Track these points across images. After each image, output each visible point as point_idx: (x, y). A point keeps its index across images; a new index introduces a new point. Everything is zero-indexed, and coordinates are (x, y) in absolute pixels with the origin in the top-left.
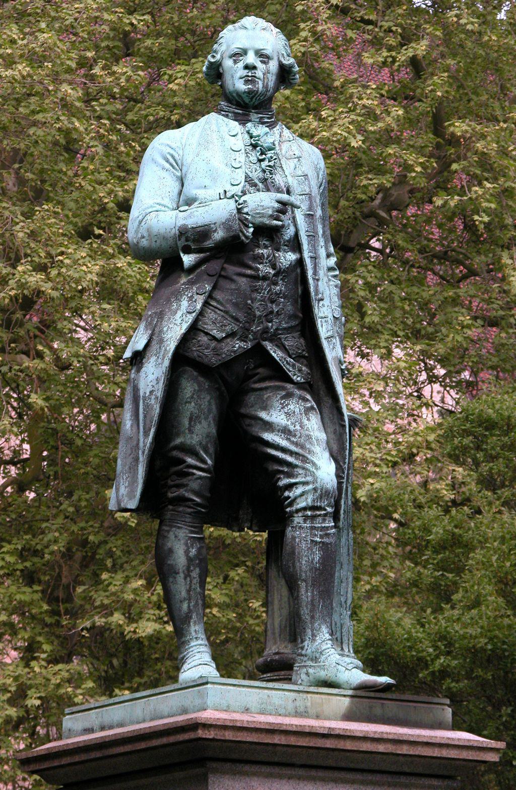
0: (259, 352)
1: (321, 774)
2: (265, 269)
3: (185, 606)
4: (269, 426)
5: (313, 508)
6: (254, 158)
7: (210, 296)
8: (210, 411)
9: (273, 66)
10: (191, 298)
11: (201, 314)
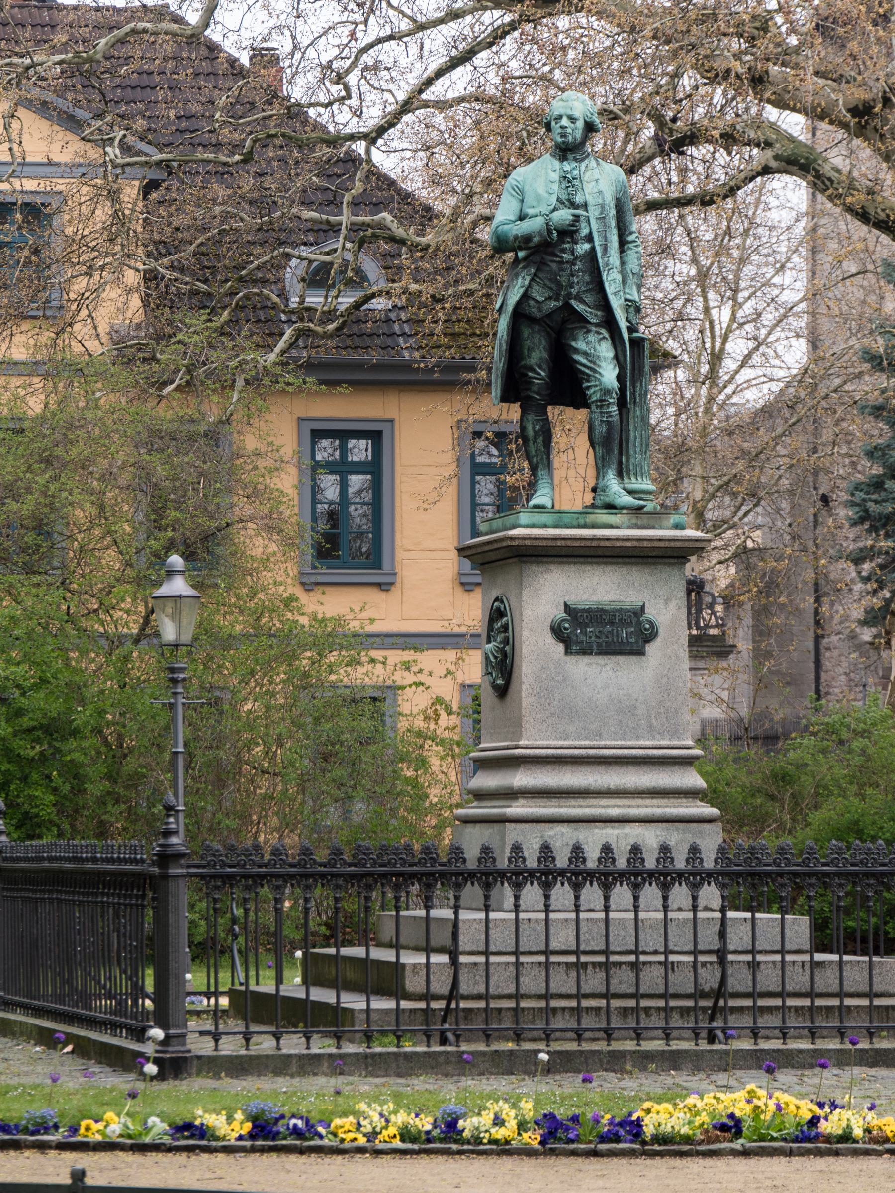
0: (567, 306)
1: (594, 560)
2: (567, 256)
4: (577, 351)
5: (601, 401)
6: (563, 186)
7: (535, 275)
8: (540, 343)
9: (580, 124)
11: (530, 286)
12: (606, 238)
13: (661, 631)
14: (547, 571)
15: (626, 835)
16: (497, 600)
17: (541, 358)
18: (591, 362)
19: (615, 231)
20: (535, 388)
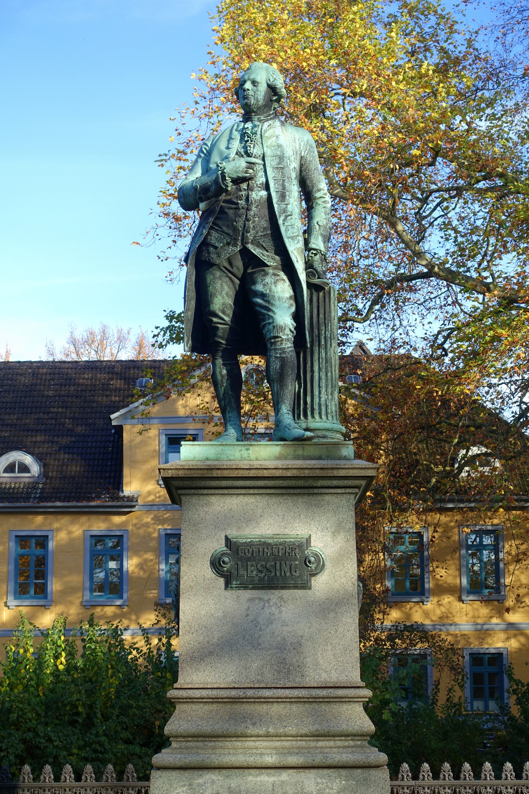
12: (284, 188)
13: (327, 564)
15: (283, 782)
17: (224, 304)
20: (220, 333)
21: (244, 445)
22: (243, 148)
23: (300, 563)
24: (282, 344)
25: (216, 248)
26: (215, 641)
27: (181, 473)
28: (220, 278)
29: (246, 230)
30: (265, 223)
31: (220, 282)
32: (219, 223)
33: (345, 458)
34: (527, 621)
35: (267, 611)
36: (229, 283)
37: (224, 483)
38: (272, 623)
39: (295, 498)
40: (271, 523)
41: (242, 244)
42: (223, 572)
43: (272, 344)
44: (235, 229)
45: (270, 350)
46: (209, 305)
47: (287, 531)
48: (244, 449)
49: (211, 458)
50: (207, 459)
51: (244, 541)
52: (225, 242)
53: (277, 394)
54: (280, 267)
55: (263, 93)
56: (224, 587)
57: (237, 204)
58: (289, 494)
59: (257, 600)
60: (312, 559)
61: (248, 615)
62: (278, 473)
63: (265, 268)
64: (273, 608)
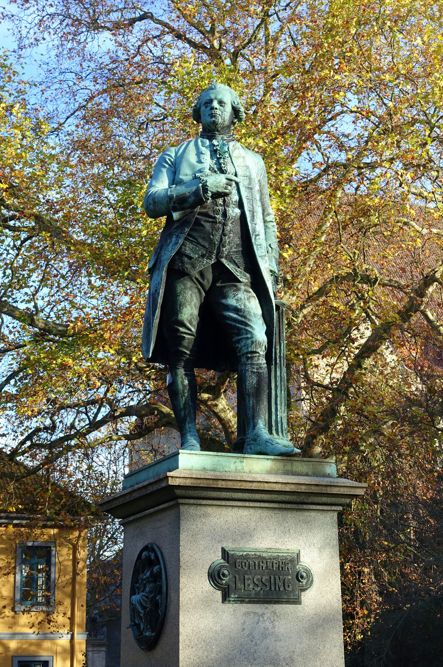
3: (183, 413)
4: (228, 308)
10: (177, 236)
13: (315, 579)
14: (205, 515)
16: (146, 548)
18: (242, 316)
19: (259, 204)
20: (185, 343)
21: (238, 457)
22: (216, 164)
23: (292, 578)
24: (259, 359)
25: (190, 258)
26: (214, 655)
27: (188, 483)
28: (190, 289)
29: (222, 243)
30: (237, 240)
31: (190, 292)
32: (194, 234)
33: (329, 476)
34: (185, 654)
35: (261, 625)
36: (198, 294)
37: (224, 495)
38: (266, 638)
39: (285, 513)
40: (269, 537)
41: (217, 258)
42: (222, 584)
43: (248, 358)
44: (211, 242)
45: (246, 364)
46: (177, 315)
47: (278, 546)
48: (238, 461)
49: (208, 468)
50: (204, 469)
51: (241, 553)
52: (200, 253)
53: (253, 408)
54: (249, 284)
55: (229, 114)
56: (221, 600)
57: (215, 218)
58: (280, 509)
59: (252, 615)
60: (304, 574)
61: (244, 629)
62: (278, 487)
63: (238, 284)
64: (267, 623)
